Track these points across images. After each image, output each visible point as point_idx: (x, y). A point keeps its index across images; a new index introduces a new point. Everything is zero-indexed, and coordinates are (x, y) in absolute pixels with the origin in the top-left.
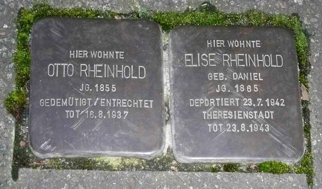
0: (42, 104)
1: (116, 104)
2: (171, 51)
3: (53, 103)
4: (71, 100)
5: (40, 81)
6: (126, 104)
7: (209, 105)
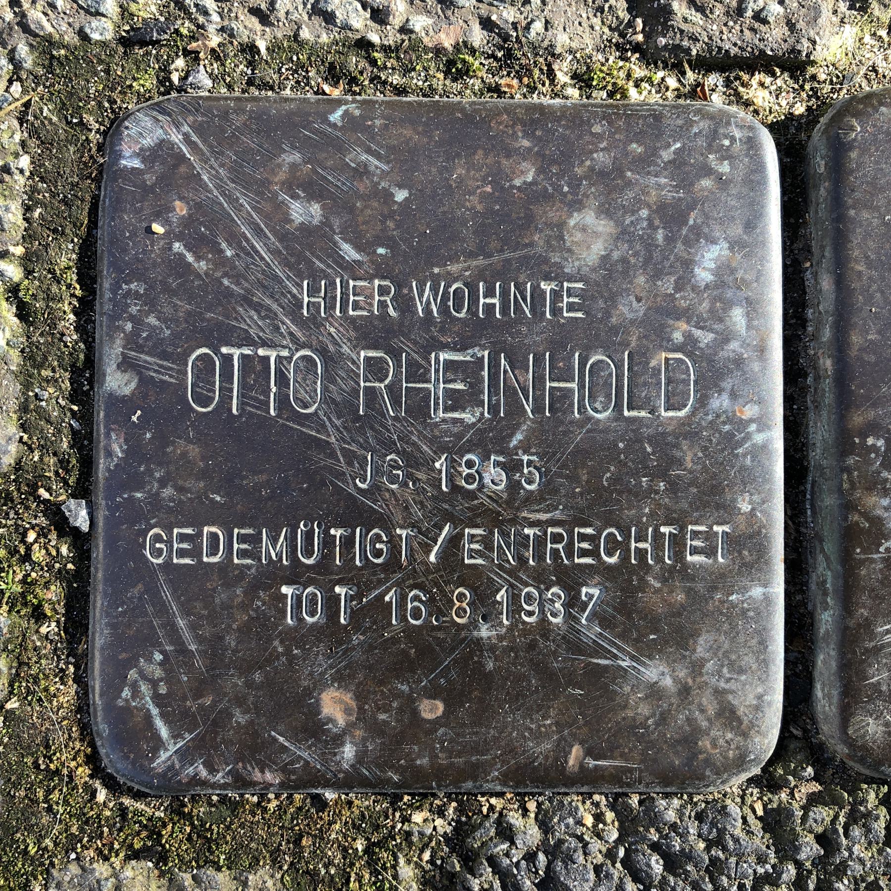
0: (158, 553)
1: (540, 556)
2: (828, 249)
3: (214, 551)
4: (309, 535)
5: (148, 436)
6: (594, 553)
7: (324, 557)
